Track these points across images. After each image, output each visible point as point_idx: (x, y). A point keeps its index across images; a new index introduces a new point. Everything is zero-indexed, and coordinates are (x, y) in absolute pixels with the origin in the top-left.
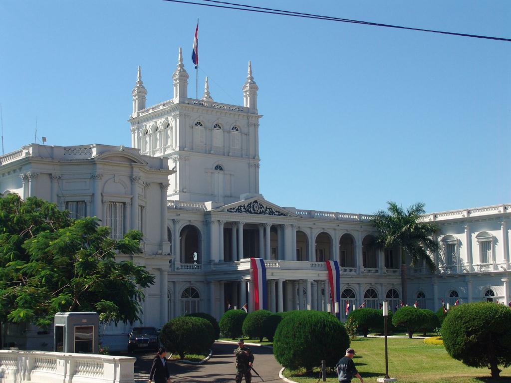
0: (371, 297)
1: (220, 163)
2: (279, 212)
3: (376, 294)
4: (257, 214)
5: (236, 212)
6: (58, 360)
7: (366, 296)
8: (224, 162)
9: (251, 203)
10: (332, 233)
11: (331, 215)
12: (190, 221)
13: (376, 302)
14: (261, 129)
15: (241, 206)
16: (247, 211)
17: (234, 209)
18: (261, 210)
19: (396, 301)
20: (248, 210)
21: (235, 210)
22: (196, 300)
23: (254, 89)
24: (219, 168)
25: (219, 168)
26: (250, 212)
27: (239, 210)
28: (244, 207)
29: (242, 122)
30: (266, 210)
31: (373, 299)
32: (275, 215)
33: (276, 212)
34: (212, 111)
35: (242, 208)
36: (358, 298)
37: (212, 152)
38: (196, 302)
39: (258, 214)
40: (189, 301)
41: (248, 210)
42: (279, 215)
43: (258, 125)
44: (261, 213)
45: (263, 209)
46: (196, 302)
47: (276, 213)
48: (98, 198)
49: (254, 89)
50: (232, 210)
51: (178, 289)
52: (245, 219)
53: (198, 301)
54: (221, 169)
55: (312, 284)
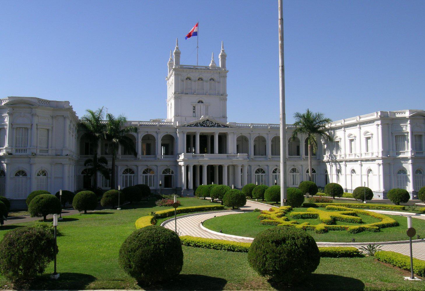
0: (260, 173)
1: (201, 99)
2: (224, 126)
3: (264, 171)
4: (208, 127)
5: (194, 126)
6: (381, 198)
7: (256, 172)
8: (204, 98)
9: (204, 121)
10: (265, 136)
11: (292, 126)
12: (259, 134)
13: (314, 176)
14: (228, 80)
15: (198, 123)
16: (202, 125)
17: (193, 125)
18: (212, 125)
19: (263, 175)
20: (202, 125)
21: (194, 125)
22: (132, 175)
23: (224, 57)
24: (201, 102)
25: (201, 102)
26: (204, 126)
27: (196, 125)
28: (200, 123)
29: (216, 77)
30: (215, 125)
31: (262, 174)
32: (221, 127)
33: (222, 125)
34: (202, 71)
35: (199, 124)
36: (267, 174)
37: (195, 94)
38: (314, 175)
39: (209, 127)
40: (147, 176)
41: (202, 125)
42: (224, 127)
43: (226, 77)
44: (211, 126)
45: (213, 124)
46: (314, 175)
47: (222, 126)
48: (35, 127)
49: (224, 56)
50: (192, 126)
51: (270, 168)
52: (200, 131)
53: (315, 175)
54: (202, 102)
55: (228, 167)
